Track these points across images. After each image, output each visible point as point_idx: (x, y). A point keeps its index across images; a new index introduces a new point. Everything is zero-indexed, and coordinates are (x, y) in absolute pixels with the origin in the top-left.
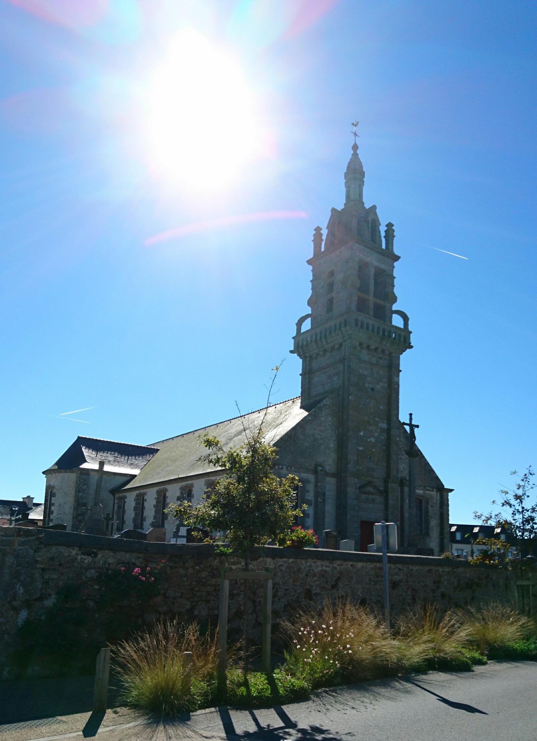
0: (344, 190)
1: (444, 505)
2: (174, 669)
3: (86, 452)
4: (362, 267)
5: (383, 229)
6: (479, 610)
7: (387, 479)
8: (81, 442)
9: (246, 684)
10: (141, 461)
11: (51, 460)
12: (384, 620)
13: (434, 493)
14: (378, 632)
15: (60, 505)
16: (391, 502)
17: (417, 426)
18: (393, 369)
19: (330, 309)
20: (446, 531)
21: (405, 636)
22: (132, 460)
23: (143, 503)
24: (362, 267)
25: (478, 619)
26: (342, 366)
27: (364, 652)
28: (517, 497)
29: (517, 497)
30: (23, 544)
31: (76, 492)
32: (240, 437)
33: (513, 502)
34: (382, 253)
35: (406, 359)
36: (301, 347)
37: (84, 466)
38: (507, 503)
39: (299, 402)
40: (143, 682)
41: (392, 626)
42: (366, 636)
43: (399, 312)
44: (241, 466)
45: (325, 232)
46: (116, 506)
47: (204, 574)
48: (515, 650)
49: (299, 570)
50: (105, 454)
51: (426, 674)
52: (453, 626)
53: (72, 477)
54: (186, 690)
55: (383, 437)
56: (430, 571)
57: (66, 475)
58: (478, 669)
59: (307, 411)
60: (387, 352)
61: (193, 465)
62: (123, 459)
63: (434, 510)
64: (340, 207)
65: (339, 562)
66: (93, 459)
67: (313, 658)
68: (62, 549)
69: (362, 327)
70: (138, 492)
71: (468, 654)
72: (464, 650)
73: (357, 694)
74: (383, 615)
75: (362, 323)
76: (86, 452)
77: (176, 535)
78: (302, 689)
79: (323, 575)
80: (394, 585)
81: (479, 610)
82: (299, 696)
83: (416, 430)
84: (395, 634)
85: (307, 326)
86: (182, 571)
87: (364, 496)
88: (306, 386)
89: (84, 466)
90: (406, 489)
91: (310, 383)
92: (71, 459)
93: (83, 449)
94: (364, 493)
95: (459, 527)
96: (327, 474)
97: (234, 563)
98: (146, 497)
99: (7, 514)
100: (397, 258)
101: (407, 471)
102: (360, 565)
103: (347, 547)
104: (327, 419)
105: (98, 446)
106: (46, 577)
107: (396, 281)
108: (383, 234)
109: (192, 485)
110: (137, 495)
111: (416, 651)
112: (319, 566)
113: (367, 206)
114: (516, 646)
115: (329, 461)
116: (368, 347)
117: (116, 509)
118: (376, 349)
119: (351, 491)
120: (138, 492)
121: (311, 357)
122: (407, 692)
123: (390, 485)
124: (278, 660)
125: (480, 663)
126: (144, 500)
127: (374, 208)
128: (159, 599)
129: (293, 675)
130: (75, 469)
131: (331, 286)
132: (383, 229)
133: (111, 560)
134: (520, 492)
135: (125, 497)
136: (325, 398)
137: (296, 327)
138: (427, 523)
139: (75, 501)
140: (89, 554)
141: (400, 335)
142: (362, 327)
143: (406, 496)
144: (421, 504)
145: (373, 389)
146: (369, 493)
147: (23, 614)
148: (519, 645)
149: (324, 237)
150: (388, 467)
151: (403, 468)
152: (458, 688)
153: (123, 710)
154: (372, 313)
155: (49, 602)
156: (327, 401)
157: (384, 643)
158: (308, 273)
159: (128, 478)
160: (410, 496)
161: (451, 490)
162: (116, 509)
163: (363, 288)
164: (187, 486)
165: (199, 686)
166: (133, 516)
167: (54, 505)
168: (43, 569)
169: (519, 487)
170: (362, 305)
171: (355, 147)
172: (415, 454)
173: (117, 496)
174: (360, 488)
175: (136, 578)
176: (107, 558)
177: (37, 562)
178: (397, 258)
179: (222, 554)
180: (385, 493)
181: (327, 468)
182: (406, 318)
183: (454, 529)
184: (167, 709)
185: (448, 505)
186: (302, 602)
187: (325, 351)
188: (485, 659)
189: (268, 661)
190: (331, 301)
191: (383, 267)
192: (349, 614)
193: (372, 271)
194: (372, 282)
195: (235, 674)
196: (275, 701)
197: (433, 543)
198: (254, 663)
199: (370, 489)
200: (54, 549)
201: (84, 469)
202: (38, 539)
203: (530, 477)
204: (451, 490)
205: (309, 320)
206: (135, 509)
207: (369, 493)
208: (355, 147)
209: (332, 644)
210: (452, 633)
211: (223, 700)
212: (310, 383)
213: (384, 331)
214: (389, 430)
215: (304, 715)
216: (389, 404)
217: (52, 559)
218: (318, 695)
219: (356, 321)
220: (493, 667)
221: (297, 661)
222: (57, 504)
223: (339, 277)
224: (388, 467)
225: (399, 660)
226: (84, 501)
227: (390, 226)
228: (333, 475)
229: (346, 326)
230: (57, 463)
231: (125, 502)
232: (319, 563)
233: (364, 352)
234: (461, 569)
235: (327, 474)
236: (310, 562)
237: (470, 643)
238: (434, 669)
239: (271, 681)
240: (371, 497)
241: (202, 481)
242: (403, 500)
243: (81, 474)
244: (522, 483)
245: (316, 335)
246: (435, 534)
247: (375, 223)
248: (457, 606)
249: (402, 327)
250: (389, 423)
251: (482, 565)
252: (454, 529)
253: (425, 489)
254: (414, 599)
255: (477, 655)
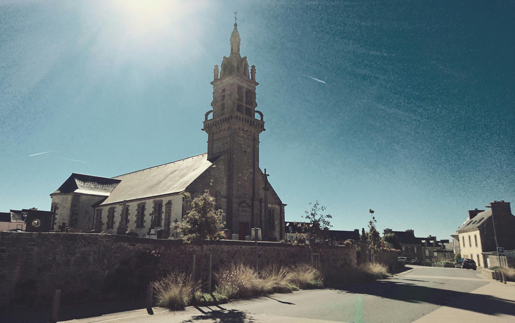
0: (230, 47)
1: (282, 213)
2: (174, 291)
3: (78, 182)
4: (240, 88)
5: (250, 68)
6: (296, 267)
7: (253, 199)
8: (74, 176)
9: (203, 297)
10: (110, 187)
11: (55, 187)
12: (256, 271)
13: (277, 207)
14: (254, 276)
15: (61, 214)
16: (255, 211)
17: (268, 175)
18: (256, 141)
19: (223, 109)
20: (283, 226)
21: (264, 278)
22: (105, 186)
23: (113, 214)
24: (240, 88)
25: (296, 271)
26: (229, 139)
27: (248, 285)
28: (312, 214)
29: (312, 214)
30: (107, 241)
31: (71, 206)
32: (173, 175)
33: (310, 216)
34: (249, 81)
35: (262, 136)
36: (208, 127)
37: (77, 191)
38: (308, 217)
39: (206, 156)
40: (166, 296)
41: (259, 273)
42: (248, 277)
43: (257, 112)
44: (199, 206)
45: (220, 69)
46: (95, 215)
47: (178, 253)
48: (311, 284)
49: (218, 250)
50: (89, 184)
51: (273, 294)
52: (284, 273)
53: (70, 197)
54: (182, 299)
55: (251, 176)
56: (275, 249)
57: (65, 196)
58: (294, 292)
59: (211, 162)
60: (253, 132)
61: (145, 191)
62: (100, 186)
63: (277, 216)
64: (228, 56)
65: (235, 246)
66: (82, 186)
67: (227, 288)
68: (122, 243)
69: (240, 119)
70: (110, 206)
71: (291, 286)
72: (289, 285)
73: (245, 301)
74: (255, 268)
75: (240, 117)
76: (78, 182)
77: (149, 233)
78: (225, 299)
79: (228, 252)
80: (259, 256)
81: (296, 267)
82: (224, 301)
83: (268, 177)
84: (260, 277)
85: (210, 117)
86: (169, 252)
87: (241, 209)
88: (211, 148)
89: (77, 191)
90: (263, 204)
91: (212, 147)
92: (68, 187)
93: (76, 181)
94: (242, 207)
95: (291, 223)
96: (222, 197)
97: (190, 248)
98: (115, 210)
99: (20, 219)
100: (258, 84)
101: (263, 195)
102: (244, 247)
103: (235, 239)
104: (222, 167)
105: (85, 179)
106: (116, 255)
107: (257, 96)
108: (250, 71)
109: (145, 203)
110: (110, 208)
111: (269, 284)
112: (226, 248)
113: (242, 56)
114: (312, 283)
115: (223, 189)
116: (243, 130)
117: (95, 216)
118: (247, 131)
119: (235, 206)
120: (110, 206)
121: (213, 133)
122: (266, 300)
123: (255, 202)
124: (214, 289)
125: (295, 290)
126: (114, 211)
127: (245, 58)
128: (160, 265)
129: (221, 294)
130: (72, 193)
131: (223, 97)
132: (250, 68)
133: (141, 248)
134: (313, 212)
135: (102, 209)
136: (221, 156)
137: (204, 117)
138: (274, 222)
139: (71, 212)
140: (132, 245)
141: (259, 124)
142: (240, 119)
143: (263, 208)
144: (271, 213)
145: (245, 151)
146: (244, 207)
147: (107, 272)
148: (313, 282)
149: (220, 71)
150: (254, 192)
151: (262, 193)
152: (285, 297)
153: (158, 308)
154: (244, 112)
155: (117, 266)
156: (222, 157)
157: (256, 280)
158: (211, 89)
159: (102, 198)
160: (265, 207)
161: (286, 205)
162: (95, 216)
163: (240, 99)
164: (142, 203)
165: (186, 299)
166: (107, 221)
167: (57, 214)
168: (114, 252)
169: (313, 210)
170: (239, 108)
171: (236, 25)
172: (268, 187)
173: (96, 209)
174: (239, 204)
175: (153, 255)
176: (140, 246)
177: (112, 249)
178: (258, 84)
179: (186, 243)
180: (252, 207)
181: (222, 193)
182: (262, 115)
183: (288, 224)
184: (175, 306)
185: (284, 213)
186: (224, 263)
187: (221, 130)
188: (298, 288)
189: (210, 289)
190: (223, 105)
191: (250, 88)
192: (241, 269)
193: (245, 90)
194: (245, 96)
195: (198, 293)
196: (215, 303)
197: (277, 234)
198: (205, 290)
199: (244, 205)
200: (119, 243)
201: (77, 193)
202: (113, 239)
203: (317, 205)
204: (286, 205)
205: (212, 113)
206: (108, 216)
207: (244, 207)
208: (236, 25)
209: (235, 281)
210: (284, 277)
211: (196, 303)
212: (212, 147)
213: (251, 121)
214: (254, 173)
215: (228, 307)
216: (254, 157)
217: (118, 248)
218: (231, 302)
219: (237, 117)
220: (301, 291)
221: (221, 289)
222: (59, 214)
223: (227, 93)
224: (254, 192)
225: (262, 288)
226: (76, 212)
227: (253, 67)
228: (225, 197)
229: (231, 119)
230: (60, 189)
231: (101, 213)
232: (227, 246)
233: (241, 132)
234: (289, 248)
235: (222, 197)
236: (223, 246)
237: (292, 281)
238: (276, 292)
239: (213, 296)
240: (245, 209)
241: (152, 200)
242: (261, 211)
243: (75, 195)
244: (314, 208)
245: (216, 122)
246: (277, 229)
247: (246, 65)
248: (287, 265)
249: (260, 119)
250: (254, 169)
251: (298, 246)
252: (288, 224)
253: (272, 204)
254: (268, 262)
255: (294, 287)
